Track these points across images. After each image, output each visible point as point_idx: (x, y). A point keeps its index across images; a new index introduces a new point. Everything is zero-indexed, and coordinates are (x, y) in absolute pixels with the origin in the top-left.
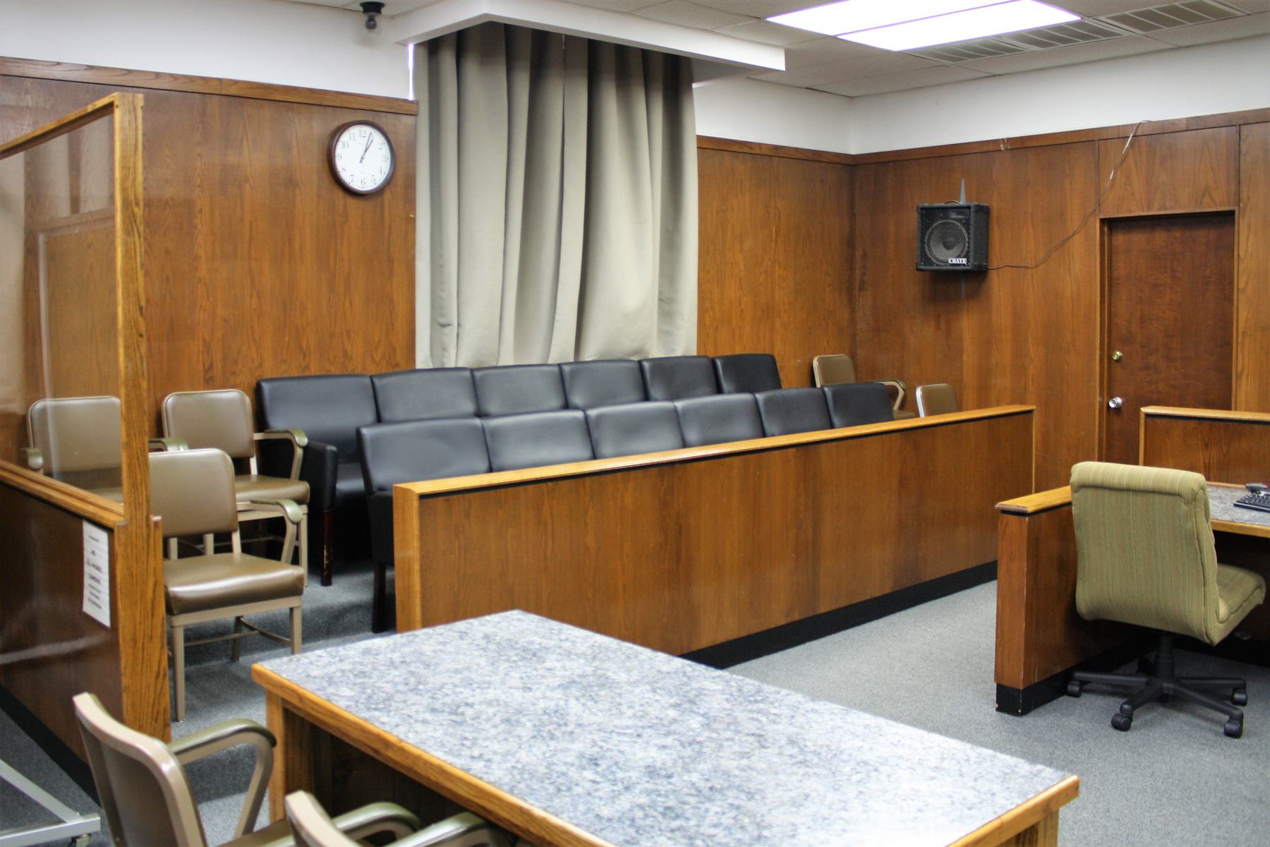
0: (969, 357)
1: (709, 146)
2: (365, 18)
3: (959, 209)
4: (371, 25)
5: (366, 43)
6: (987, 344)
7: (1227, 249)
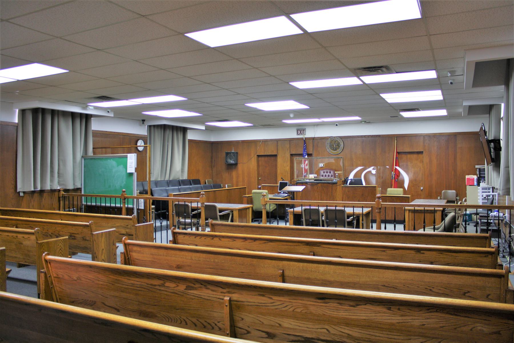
0: (234, 179)
1: (190, 141)
2: (142, 122)
3: (233, 153)
4: (143, 123)
5: (140, 125)
6: (238, 177)
7: (276, 160)
